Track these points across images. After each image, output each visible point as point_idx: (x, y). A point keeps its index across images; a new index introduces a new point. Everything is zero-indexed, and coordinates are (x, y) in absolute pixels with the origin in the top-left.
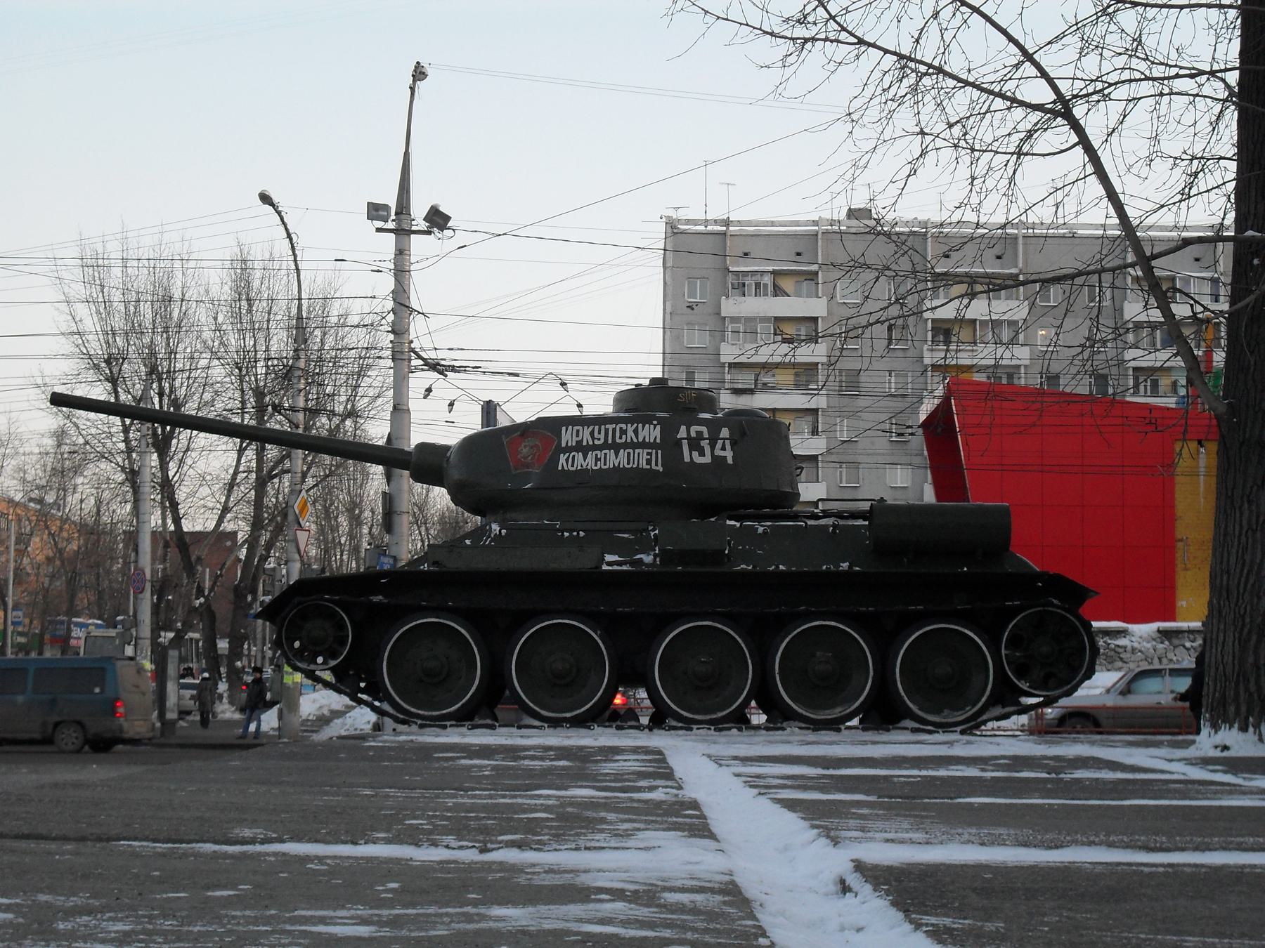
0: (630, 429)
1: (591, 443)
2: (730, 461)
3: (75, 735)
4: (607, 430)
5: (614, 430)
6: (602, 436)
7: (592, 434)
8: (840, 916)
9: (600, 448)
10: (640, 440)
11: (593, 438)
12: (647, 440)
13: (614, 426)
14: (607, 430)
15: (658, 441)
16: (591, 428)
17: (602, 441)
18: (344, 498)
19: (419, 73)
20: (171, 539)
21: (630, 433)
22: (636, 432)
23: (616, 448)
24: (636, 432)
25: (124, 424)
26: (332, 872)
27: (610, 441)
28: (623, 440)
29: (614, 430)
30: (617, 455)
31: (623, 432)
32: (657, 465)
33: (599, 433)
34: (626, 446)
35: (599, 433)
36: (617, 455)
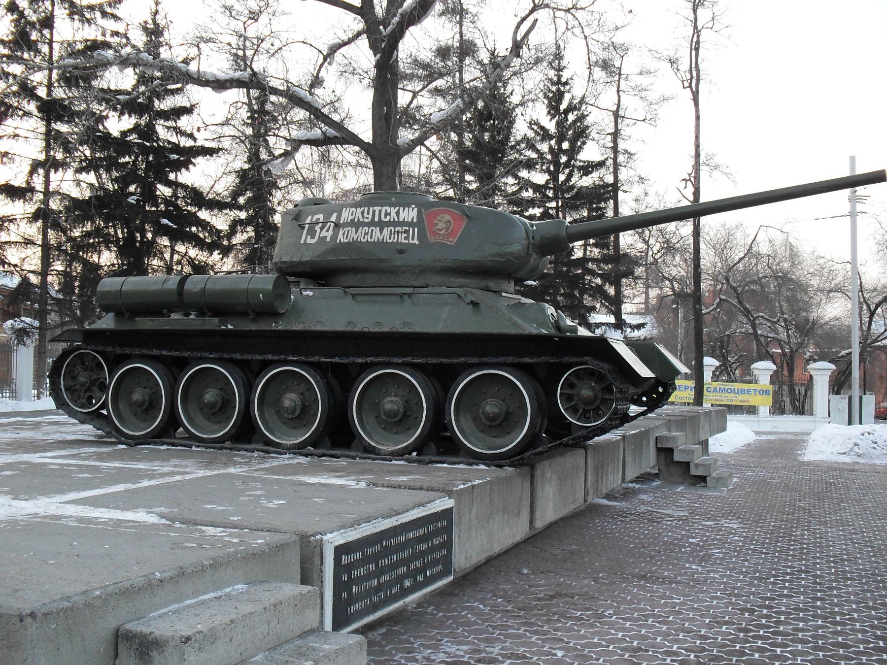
0: (393, 211)
1: (361, 220)
4: (374, 211)
5: (380, 211)
6: (370, 216)
7: (363, 213)
11: (363, 217)
12: (406, 220)
13: (380, 208)
14: (374, 211)
15: (415, 220)
16: (397, 208)
17: (370, 219)
21: (393, 215)
22: (398, 213)
23: (382, 225)
24: (398, 213)
27: (376, 219)
28: (388, 219)
29: (380, 211)
32: (413, 239)
33: (368, 213)
34: (364, 224)
35: (368, 213)
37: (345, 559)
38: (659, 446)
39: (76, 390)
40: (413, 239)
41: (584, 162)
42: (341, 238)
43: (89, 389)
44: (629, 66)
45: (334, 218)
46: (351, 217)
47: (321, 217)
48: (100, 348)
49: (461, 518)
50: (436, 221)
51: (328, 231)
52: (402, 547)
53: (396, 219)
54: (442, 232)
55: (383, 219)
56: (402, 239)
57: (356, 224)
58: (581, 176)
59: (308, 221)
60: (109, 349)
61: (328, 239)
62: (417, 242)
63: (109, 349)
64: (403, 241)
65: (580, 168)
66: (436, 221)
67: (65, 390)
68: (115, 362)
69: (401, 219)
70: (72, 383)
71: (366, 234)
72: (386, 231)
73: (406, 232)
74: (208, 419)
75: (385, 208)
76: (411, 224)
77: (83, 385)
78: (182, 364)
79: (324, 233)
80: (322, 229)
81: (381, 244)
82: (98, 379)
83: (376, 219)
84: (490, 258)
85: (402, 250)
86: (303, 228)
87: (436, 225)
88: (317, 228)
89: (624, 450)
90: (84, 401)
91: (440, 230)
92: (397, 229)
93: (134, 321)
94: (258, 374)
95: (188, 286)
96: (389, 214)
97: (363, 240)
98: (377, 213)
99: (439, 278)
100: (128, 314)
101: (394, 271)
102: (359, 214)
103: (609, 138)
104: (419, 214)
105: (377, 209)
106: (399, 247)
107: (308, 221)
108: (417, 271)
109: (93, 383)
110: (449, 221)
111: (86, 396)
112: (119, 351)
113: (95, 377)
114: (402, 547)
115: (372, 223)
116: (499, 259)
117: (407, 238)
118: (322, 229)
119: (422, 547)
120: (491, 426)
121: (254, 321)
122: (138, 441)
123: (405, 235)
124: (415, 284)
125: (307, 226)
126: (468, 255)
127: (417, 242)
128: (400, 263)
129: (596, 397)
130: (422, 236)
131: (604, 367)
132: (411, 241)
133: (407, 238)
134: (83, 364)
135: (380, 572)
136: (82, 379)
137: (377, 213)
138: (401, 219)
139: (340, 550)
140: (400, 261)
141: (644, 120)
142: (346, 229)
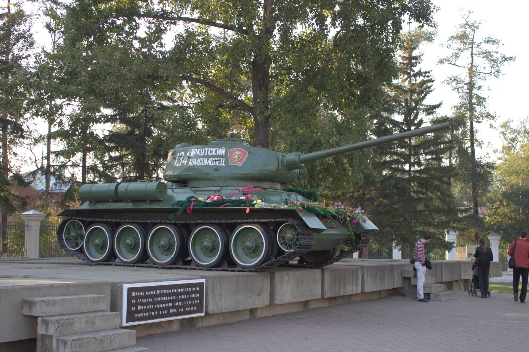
0: (214, 150)
1: (199, 154)
2: (391, 21)
3: (325, 13)
4: (205, 151)
5: (208, 150)
6: (203, 153)
7: (200, 151)
8: (489, 143)
9: (202, 157)
10: (217, 154)
11: (200, 153)
13: (208, 149)
14: (205, 151)
15: (224, 154)
18: (202, 97)
19: (36, 125)
20: (55, 125)
21: (214, 152)
22: (216, 151)
23: (208, 157)
24: (216, 151)
25: (224, 31)
26: (290, 253)
27: (206, 154)
28: (211, 154)
29: (208, 150)
30: (208, 161)
31: (211, 152)
32: (222, 164)
33: (202, 152)
35: (202, 152)
36: (208, 161)
37: (134, 294)
38: (403, 276)
39: (70, 239)
40: (222, 164)
41: (428, 106)
42: (190, 164)
43: (76, 239)
44: (479, 37)
45: (188, 155)
46: (195, 153)
47: (183, 153)
48: (81, 218)
49: (214, 290)
50: (234, 155)
51: (185, 160)
52: (171, 294)
53: (215, 154)
54: (236, 160)
55: (209, 154)
56: (217, 163)
57: (197, 157)
58: (426, 115)
59: (178, 155)
60: (85, 219)
61: (185, 164)
62: (224, 165)
63: (85, 219)
64: (218, 165)
65: (425, 110)
66: (234, 155)
67: (66, 240)
68: (88, 225)
69: (217, 154)
70: (69, 236)
71: (201, 161)
72: (210, 160)
73: (219, 160)
74: (129, 252)
75: (210, 149)
76: (222, 156)
77: (73, 237)
78: (118, 225)
79: (184, 162)
80: (183, 159)
81: (207, 166)
82: (80, 234)
83: (206, 154)
84: (258, 172)
85: (217, 169)
86: (176, 159)
87: (234, 156)
88: (181, 159)
89: (363, 276)
90: (74, 245)
91: (235, 159)
92: (215, 159)
93: (95, 205)
94: (150, 229)
95: (120, 188)
96: (212, 152)
97: (199, 165)
98: (206, 151)
99: (233, 183)
100: (94, 202)
101: (212, 179)
102: (198, 152)
103: (466, 87)
104: (226, 151)
105: (207, 149)
106: (215, 168)
107: (178, 155)
108: (223, 179)
109: (78, 236)
110: (239, 155)
111: (75, 242)
112: (89, 219)
113: (80, 233)
114: (171, 294)
115: (204, 157)
116: (262, 173)
117: (219, 163)
118: (183, 159)
119: (184, 297)
120: (250, 253)
121: (149, 204)
122: (97, 263)
123: (218, 162)
124: (222, 185)
125: (177, 158)
126: (249, 171)
127: (224, 165)
128: (215, 176)
129: (294, 238)
130: (227, 162)
131: (295, 223)
132: (221, 165)
133: (219, 163)
134: (74, 226)
135: (154, 303)
136: (72, 234)
137: (206, 151)
138: (217, 154)
139: (130, 290)
140: (216, 174)
141: (490, 73)
142: (193, 159)
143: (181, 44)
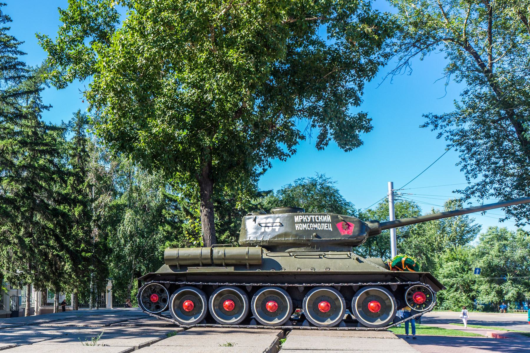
4: (311, 218)
5: (315, 218)
29: (315, 218)
34: (307, 223)
143: (114, 145)
